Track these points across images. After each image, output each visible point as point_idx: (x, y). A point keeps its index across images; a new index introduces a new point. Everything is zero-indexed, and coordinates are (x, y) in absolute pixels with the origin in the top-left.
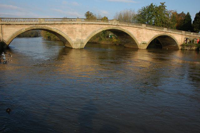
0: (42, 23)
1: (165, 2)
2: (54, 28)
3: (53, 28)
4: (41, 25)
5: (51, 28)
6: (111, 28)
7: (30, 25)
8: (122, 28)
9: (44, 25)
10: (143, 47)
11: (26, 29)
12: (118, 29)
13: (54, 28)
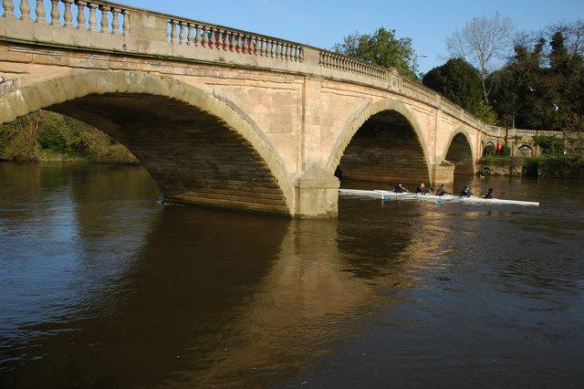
0: (152, 51)
1: (394, 31)
2: (218, 90)
3: (208, 89)
4: (147, 66)
5: (192, 91)
6: (105, 85)
7: (75, 60)
8: (408, 107)
9: (165, 68)
10: (445, 178)
11: (31, 92)
12: (165, 90)
13: (218, 90)
